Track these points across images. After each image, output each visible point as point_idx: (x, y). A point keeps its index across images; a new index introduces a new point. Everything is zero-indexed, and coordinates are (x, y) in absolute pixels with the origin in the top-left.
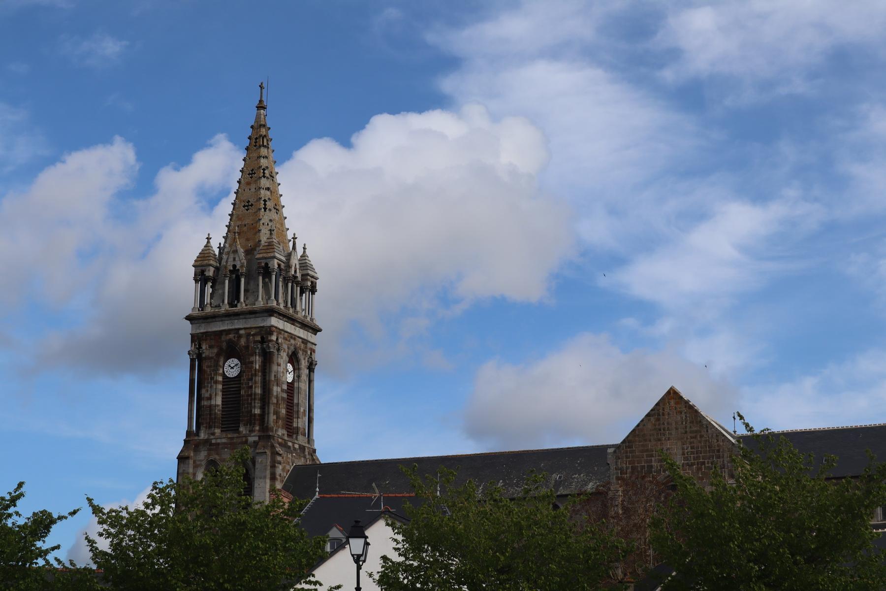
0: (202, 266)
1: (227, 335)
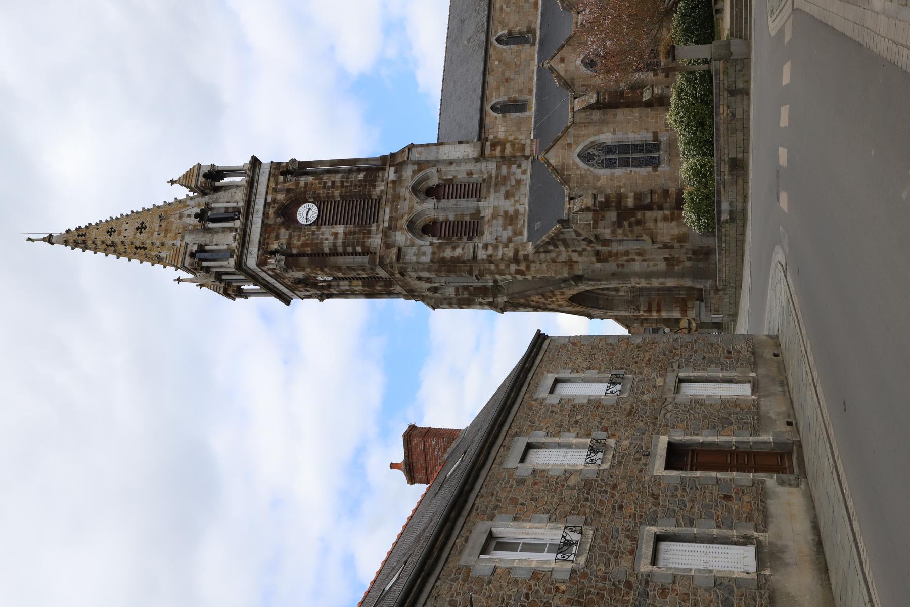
0: (185, 254)
1: (268, 218)
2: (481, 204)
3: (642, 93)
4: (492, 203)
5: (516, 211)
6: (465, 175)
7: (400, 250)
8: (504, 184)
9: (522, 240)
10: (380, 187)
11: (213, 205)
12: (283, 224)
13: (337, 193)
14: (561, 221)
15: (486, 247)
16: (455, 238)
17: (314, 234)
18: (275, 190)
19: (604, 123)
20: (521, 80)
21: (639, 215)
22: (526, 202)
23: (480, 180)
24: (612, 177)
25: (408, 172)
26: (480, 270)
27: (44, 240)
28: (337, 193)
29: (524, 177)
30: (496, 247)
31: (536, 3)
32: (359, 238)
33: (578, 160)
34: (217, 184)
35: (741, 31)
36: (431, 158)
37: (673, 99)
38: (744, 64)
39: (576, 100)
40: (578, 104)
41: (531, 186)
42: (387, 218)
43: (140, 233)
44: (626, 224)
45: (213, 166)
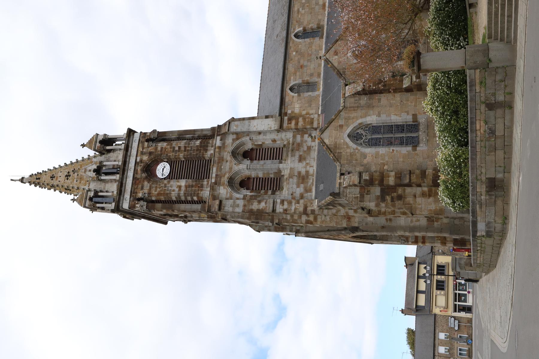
1: (137, 174)
2: (281, 166)
3: (401, 81)
4: (289, 165)
5: (307, 172)
6: (270, 142)
7: (221, 202)
8: (298, 150)
9: (311, 196)
10: (211, 151)
11: (104, 163)
12: (146, 178)
13: (181, 155)
14: (334, 194)
15: (282, 202)
16: (263, 191)
17: (165, 186)
18: (142, 153)
19: (370, 106)
20: (312, 66)
21: (400, 191)
22: (314, 164)
23: (282, 146)
24: (377, 155)
25: (229, 140)
26: (279, 219)
27: (19, 180)
28: (181, 155)
29: (313, 144)
30: (290, 203)
31: (324, 5)
32: (195, 191)
33: (348, 140)
34: (108, 148)
35: (502, 31)
36: (244, 130)
37: (429, 88)
38: (508, 72)
39: (347, 87)
40: (349, 90)
41: (319, 152)
42: (214, 175)
43: (67, 179)
44: (388, 198)
45: (105, 135)
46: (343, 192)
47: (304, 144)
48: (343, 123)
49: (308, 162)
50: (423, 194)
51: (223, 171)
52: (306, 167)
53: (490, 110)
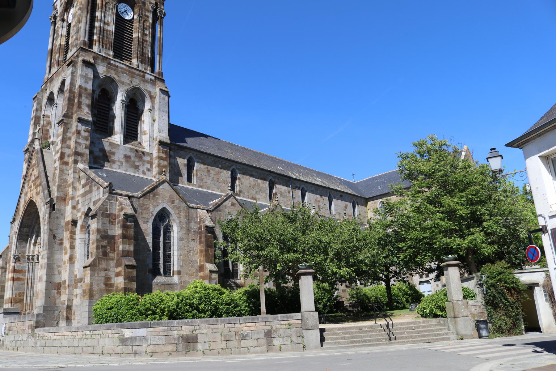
20: (209, 181)
29: (141, 172)
46: (113, 197)
47: (141, 163)
48: (175, 204)
49: (124, 164)
50: (108, 278)
51: (121, 75)
52: (119, 161)
53: (265, 334)
